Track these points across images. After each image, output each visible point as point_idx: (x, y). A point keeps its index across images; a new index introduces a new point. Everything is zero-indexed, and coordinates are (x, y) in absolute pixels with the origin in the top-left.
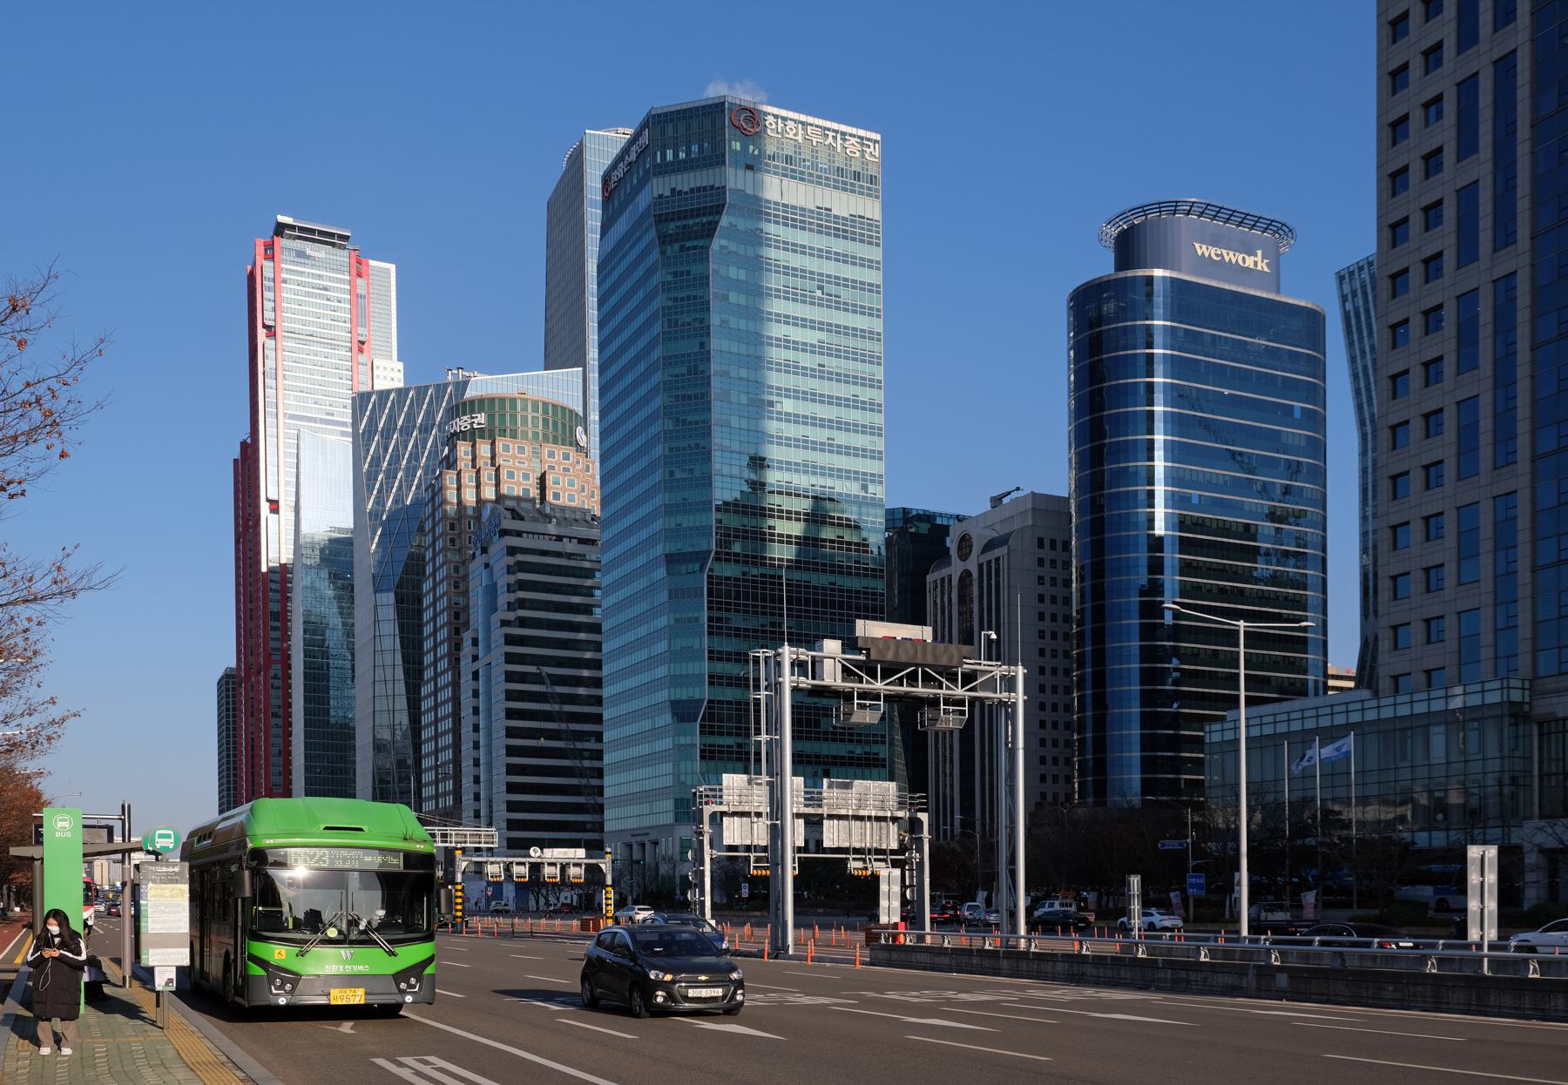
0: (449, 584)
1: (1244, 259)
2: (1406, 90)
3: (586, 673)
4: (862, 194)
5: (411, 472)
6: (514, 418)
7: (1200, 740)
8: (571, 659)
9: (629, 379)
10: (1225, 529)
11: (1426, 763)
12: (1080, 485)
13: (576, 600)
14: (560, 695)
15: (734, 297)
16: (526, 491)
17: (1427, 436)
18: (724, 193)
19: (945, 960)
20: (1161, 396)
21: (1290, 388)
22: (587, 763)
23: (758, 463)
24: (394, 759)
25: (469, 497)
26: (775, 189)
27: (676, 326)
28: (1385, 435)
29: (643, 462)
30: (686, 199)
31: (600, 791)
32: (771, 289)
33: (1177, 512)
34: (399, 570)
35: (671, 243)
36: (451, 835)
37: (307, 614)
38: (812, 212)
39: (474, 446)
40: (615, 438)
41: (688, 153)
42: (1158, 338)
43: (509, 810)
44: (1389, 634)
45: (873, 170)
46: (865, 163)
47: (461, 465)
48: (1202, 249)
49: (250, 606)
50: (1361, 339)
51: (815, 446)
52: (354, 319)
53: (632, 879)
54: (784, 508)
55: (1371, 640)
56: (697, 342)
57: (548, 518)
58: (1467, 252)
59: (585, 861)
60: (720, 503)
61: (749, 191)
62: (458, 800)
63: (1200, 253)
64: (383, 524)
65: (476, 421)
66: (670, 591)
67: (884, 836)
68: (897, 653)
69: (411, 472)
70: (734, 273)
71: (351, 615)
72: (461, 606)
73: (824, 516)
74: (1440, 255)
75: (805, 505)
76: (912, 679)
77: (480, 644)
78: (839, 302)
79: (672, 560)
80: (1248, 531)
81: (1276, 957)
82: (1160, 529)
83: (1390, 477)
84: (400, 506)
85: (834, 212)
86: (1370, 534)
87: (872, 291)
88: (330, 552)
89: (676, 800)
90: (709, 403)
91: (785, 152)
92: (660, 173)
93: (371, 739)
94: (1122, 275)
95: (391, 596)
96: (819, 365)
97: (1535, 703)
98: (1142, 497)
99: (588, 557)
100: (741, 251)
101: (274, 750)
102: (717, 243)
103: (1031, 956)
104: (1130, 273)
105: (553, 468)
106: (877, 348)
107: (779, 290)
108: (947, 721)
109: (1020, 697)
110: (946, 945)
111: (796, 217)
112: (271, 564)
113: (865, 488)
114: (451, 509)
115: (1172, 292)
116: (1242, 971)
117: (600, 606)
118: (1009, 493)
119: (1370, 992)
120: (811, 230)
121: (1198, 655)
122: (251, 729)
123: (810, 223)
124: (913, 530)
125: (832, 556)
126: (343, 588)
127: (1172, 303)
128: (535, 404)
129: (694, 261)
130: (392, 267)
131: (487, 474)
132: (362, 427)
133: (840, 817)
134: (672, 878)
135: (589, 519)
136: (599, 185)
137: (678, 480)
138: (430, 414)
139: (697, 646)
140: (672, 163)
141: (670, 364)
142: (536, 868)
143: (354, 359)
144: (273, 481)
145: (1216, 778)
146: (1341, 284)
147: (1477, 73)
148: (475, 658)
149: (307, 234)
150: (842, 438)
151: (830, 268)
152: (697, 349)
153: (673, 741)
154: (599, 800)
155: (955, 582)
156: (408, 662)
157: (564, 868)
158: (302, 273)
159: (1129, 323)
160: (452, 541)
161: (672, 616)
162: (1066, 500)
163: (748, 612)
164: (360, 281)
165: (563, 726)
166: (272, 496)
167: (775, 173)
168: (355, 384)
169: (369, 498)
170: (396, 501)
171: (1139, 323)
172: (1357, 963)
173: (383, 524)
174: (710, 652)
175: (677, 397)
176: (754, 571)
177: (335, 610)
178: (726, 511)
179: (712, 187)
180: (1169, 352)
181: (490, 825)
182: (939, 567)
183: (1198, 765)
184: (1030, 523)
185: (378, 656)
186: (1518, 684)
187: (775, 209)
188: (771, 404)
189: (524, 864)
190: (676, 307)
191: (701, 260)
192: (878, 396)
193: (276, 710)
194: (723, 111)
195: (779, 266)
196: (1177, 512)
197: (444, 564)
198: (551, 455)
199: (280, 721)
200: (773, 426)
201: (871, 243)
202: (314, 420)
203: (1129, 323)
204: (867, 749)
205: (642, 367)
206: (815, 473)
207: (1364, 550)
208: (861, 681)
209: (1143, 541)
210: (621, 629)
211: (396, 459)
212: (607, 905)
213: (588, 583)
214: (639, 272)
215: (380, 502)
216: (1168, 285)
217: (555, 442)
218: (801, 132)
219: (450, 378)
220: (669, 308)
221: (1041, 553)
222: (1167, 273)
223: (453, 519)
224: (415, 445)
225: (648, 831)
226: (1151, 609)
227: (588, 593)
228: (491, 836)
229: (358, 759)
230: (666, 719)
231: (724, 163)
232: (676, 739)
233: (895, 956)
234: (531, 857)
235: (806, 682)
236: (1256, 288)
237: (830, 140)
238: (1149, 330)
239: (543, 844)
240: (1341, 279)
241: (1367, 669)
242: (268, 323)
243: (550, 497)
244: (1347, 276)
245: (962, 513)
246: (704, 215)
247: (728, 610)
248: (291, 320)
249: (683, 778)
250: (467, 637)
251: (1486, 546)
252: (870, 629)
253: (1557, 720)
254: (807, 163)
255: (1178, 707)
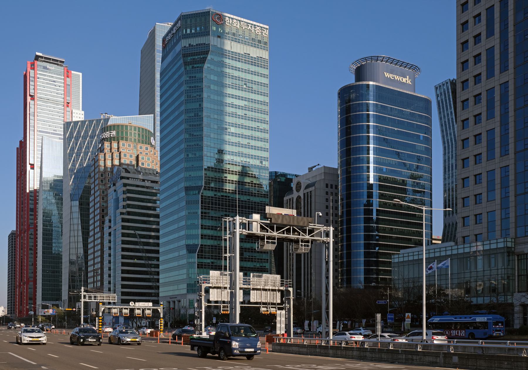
0: (100, 198)
1: (402, 79)
2: (467, 11)
3: (153, 234)
4: (262, 49)
5: (86, 154)
6: (127, 133)
7: (390, 262)
8: (147, 228)
9: (171, 118)
10: (395, 182)
11: (476, 270)
12: (342, 164)
13: (150, 205)
14: (143, 242)
15: (212, 87)
16: (131, 162)
17: (476, 144)
18: (209, 46)
19: (305, 350)
20: (372, 130)
21: (419, 128)
22: (153, 270)
23: (221, 152)
24: (77, 267)
25: (109, 164)
26: (229, 46)
27: (190, 97)
28: (460, 143)
29: (177, 150)
30: (195, 48)
31: (158, 280)
32: (227, 84)
33: (378, 174)
34: (81, 192)
35: (188, 65)
36: (98, 297)
37: (44, 210)
38: (242, 55)
39: (111, 144)
40: (166, 141)
41: (196, 30)
42: (371, 108)
43: (122, 288)
44: (461, 220)
45: (266, 40)
46: (263, 37)
47: (106, 151)
48: (387, 75)
49: (22, 206)
50: (444, 111)
51: (243, 146)
52: (65, 94)
53: (170, 315)
54: (231, 170)
55: (447, 225)
56: (198, 104)
57: (139, 173)
58: (490, 74)
59: (152, 308)
60: (206, 167)
61: (219, 46)
62: (102, 284)
63: (386, 76)
64: (75, 174)
65: (112, 134)
66: (186, 201)
67: (275, 298)
68: (282, 220)
69: (86, 154)
70: (213, 77)
71: (61, 210)
72: (105, 207)
73: (246, 173)
74: (480, 74)
75: (238, 169)
76: (288, 231)
77: (112, 222)
78: (252, 90)
79: (187, 189)
80: (404, 183)
81: (452, 349)
82: (372, 181)
83: (474, 155)
84: (82, 167)
85: (251, 55)
86: (447, 185)
87: (265, 86)
88: (54, 185)
89: (188, 284)
90: (203, 128)
91: (233, 31)
92: (185, 38)
93: (68, 259)
94: (358, 83)
95: (78, 202)
96: (245, 114)
97: (516, 247)
98: (365, 168)
99: (154, 188)
100: (216, 69)
101: (30, 263)
102: (206, 66)
103: (342, 348)
104: (361, 83)
105: (141, 153)
106: (267, 108)
107: (229, 85)
108: (302, 249)
109: (331, 240)
110: (305, 343)
111: (237, 57)
112: (30, 189)
113: (261, 162)
114: (102, 168)
115: (376, 90)
116: (437, 355)
117: (159, 207)
118: (315, 166)
119: (496, 365)
120: (242, 62)
121: (385, 230)
122: (21, 255)
123: (242, 59)
124: (279, 180)
125: (249, 189)
126: (59, 199)
127: (376, 95)
128: (135, 128)
129: (198, 72)
130: (81, 74)
131: (116, 155)
132: (67, 135)
133: (257, 289)
134: (185, 315)
135: (155, 173)
136: (161, 42)
137: (190, 158)
138: (94, 131)
139: (196, 223)
140: (189, 34)
141: (188, 112)
142: (132, 310)
143: (65, 109)
144: (32, 157)
145: (396, 277)
146: (436, 90)
147: (493, 5)
148: (110, 227)
149: (47, 60)
150: (253, 143)
151: (249, 77)
152: (198, 107)
153: (187, 261)
154: (158, 284)
155: (295, 200)
156: (84, 229)
157: (143, 310)
158: (45, 75)
159: (360, 102)
160: (102, 181)
161: (187, 211)
162: (337, 170)
163: (216, 210)
164: (68, 79)
165: (144, 255)
166: (32, 162)
167: (229, 39)
168: (65, 119)
169: (69, 164)
170: (80, 165)
171: (364, 102)
172: (473, 351)
173: (75, 174)
174: (201, 225)
175: (190, 125)
176: (219, 194)
177: (56, 208)
178: (208, 170)
179: (204, 44)
180: (375, 113)
181: (115, 293)
182: (288, 195)
183: (389, 272)
184: (323, 178)
185: (72, 226)
186: (510, 240)
187: (228, 53)
188: (226, 129)
189: (127, 309)
190: (190, 90)
191: (200, 72)
192: (266, 127)
193: (31, 247)
194: (209, 15)
195: (230, 75)
196: (378, 174)
197: (98, 190)
198: (141, 148)
199: (33, 252)
200: (227, 138)
201: (265, 68)
202: (49, 133)
203: (360, 102)
204: (261, 265)
205: (177, 113)
206: (242, 156)
207: (445, 191)
208: (268, 232)
209: (365, 186)
210: (167, 216)
211: (80, 149)
212: (161, 326)
213: (155, 198)
214: (176, 76)
215: (74, 165)
216: (375, 87)
217: (143, 143)
218: (239, 24)
219: (102, 117)
220: (188, 90)
221: (327, 190)
222: (374, 83)
223: (102, 172)
224: (88, 143)
225: (177, 296)
226: (368, 212)
227: (154, 202)
228: (114, 297)
229: (63, 267)
230: (184, 252)
231: (209, 35)
232: (188, 260)
233: (283, 348)
234: (130, 306)
235: (245, 232)
236: (407, 90)
237: (250, 27)
238: (368, 105)
239: (135, 301)
240: (436, 88)
241: (446, 236)
242: (31, 94)
243: (140, 164)
244: (438, 87)
245: (297, 174)
246: (201, 55)
247: (208, 209)
248: (41, 94)
249: (190, 276)
250: (107, 219)
251: (498, 187)
252: (271, 210)
253: (524, 254)
254: (241, 36)
255: (378, 250)
